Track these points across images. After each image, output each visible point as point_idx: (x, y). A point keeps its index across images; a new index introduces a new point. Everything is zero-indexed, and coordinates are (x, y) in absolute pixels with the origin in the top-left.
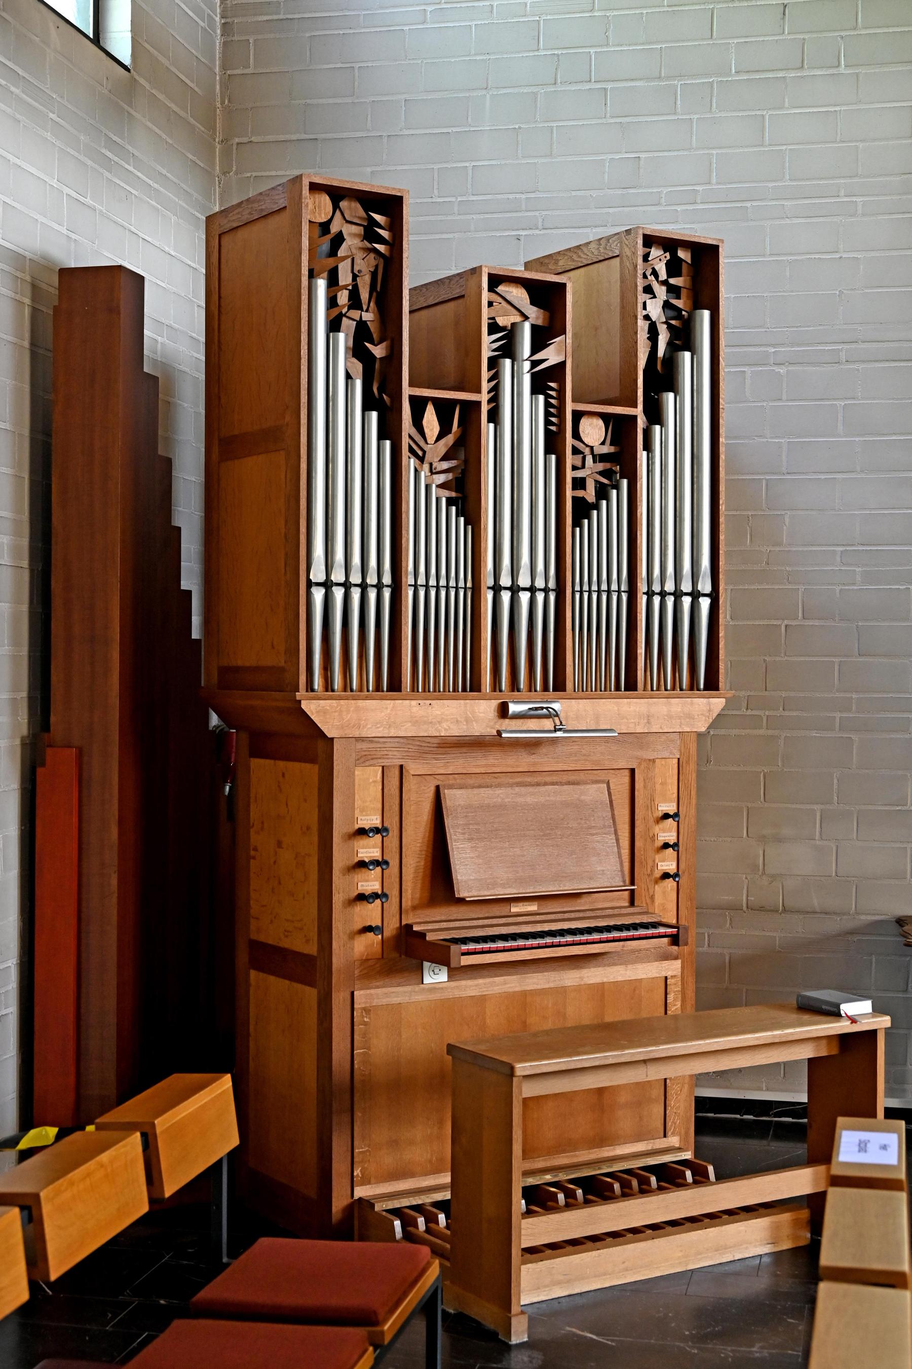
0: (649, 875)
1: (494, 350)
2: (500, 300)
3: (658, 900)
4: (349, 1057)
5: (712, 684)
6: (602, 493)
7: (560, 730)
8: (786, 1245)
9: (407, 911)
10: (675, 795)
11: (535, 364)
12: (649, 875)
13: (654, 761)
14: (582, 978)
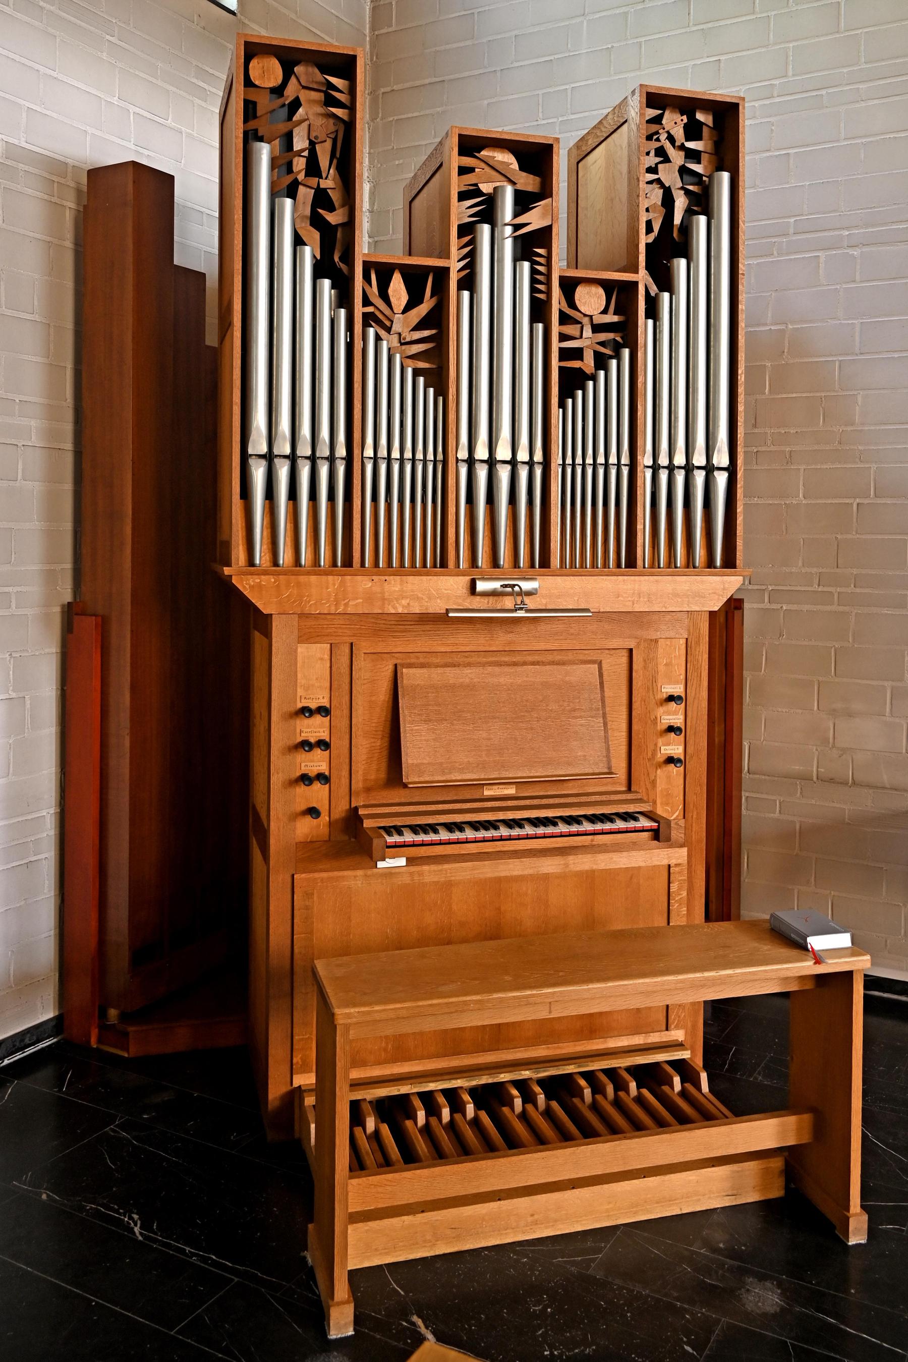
0: (649, 760)
1: (470, 216)
2: (483, 165)
3: (661, 785)
4: (289, 942)
5: (730, 562)
6: (601, 362)
7: (521, 609)
8: (752, 1197)
9: (358, 794)
10: (683, 677)
11: (517, 227)
12: (649, 760)
13: (656, 641)
14: (567, 865)
